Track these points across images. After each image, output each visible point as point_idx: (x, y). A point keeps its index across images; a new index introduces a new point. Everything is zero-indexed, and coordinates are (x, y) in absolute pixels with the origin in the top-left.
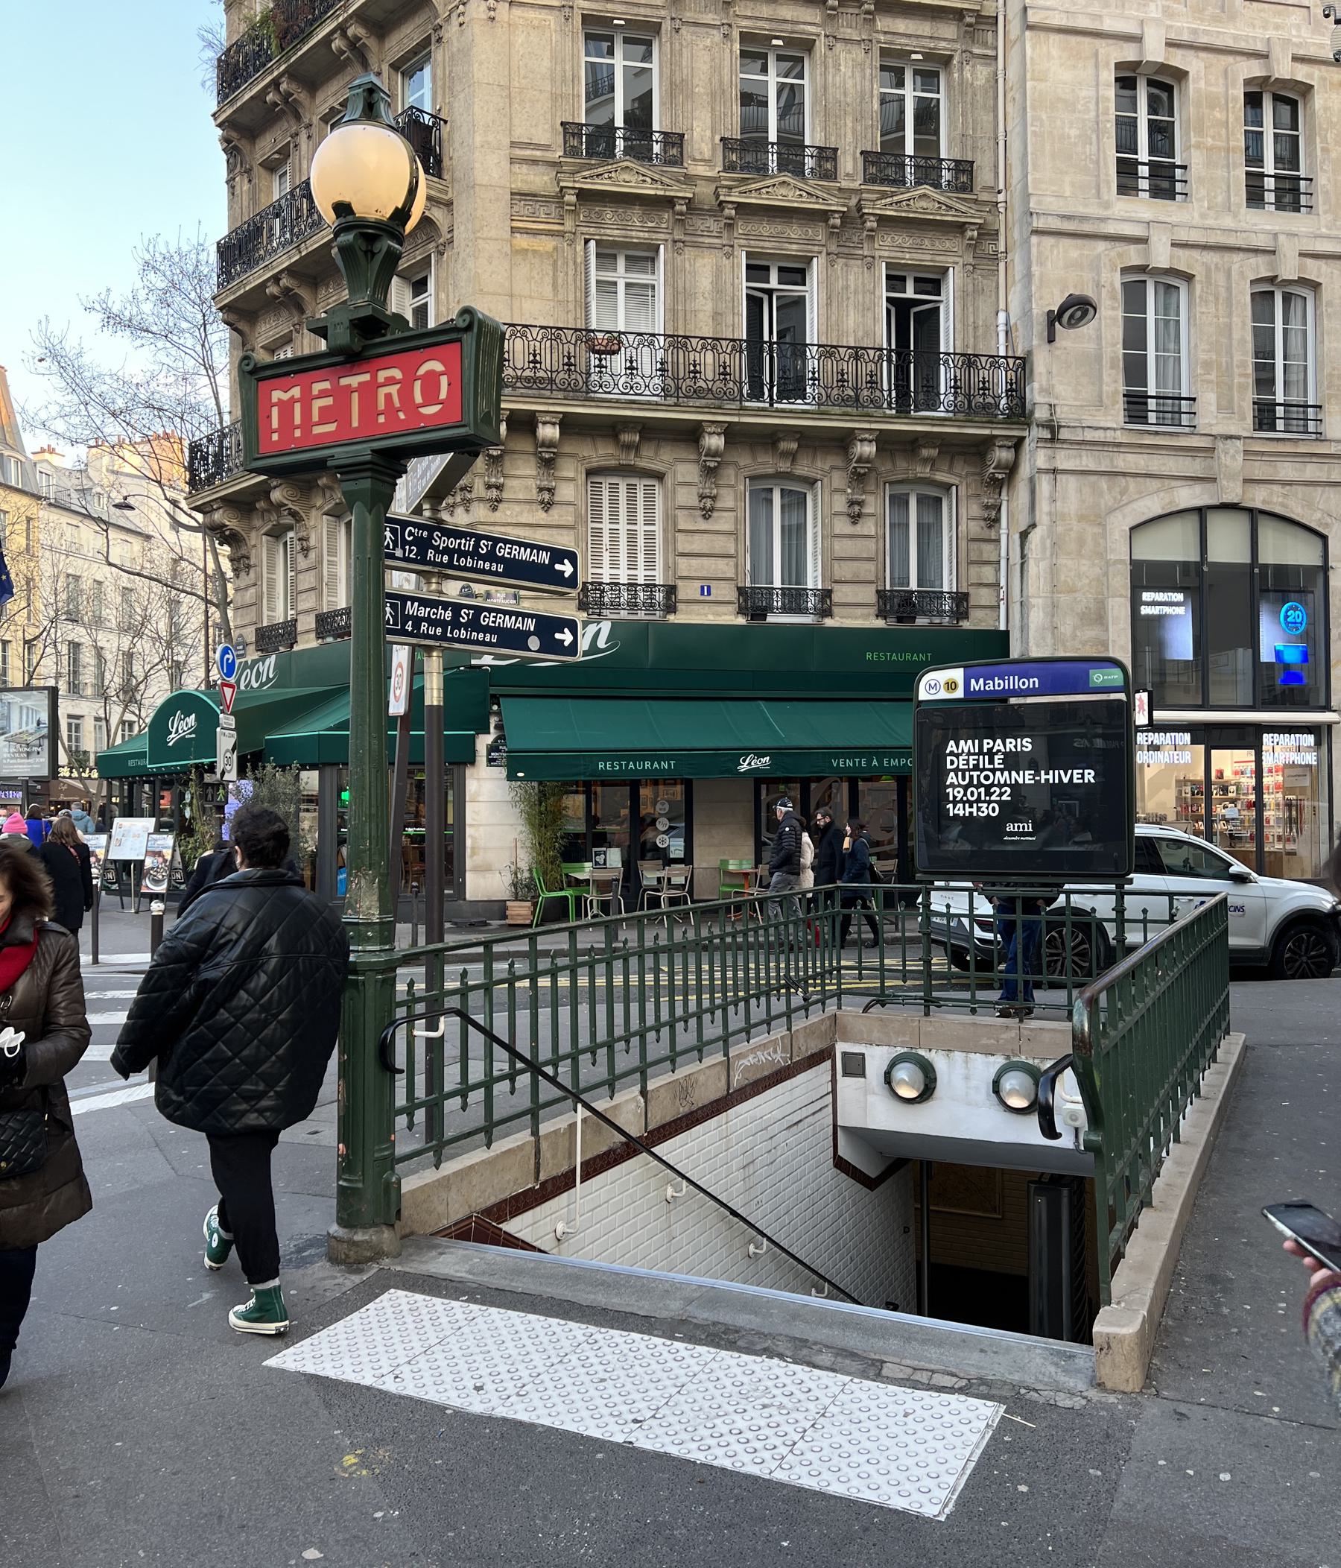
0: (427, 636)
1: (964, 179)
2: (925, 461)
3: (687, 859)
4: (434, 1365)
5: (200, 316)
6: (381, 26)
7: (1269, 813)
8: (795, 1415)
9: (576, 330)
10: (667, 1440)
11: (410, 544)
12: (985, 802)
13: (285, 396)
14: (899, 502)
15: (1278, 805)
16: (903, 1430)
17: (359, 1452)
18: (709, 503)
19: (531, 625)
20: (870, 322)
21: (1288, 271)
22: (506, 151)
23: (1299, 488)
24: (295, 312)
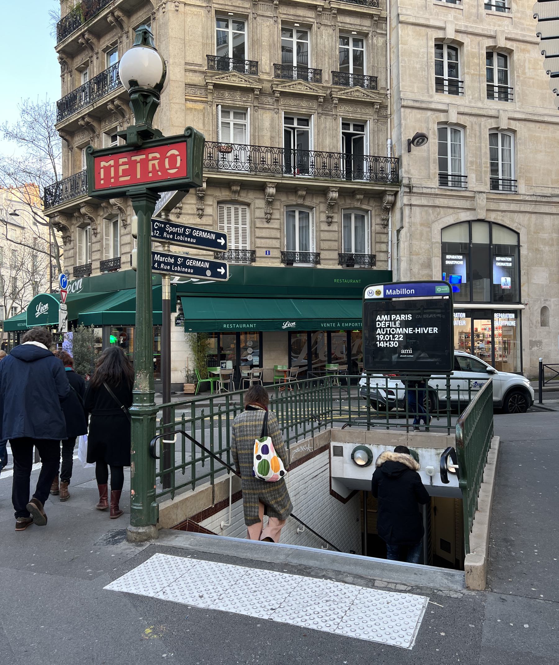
0: (164, 270)
1: (373, 84)
2: (358, 200)
3: (260, 365)
4: (190, 588)
5: (47, 134)
6: (129, 12)
7: (496, 346)
8: (340, 605)
9: (213, 142)
10: (287, 617)
11: (157, 230)
12: (392, 341)
13: (107, 164)
14: (347, 217)
15: (500, 342)
16: (387, 607)
17: (152, 627)
18: (269, 216)
19: (207, 265)
20: (335, 142)
21: (504, 126)
22: (183, 67)
23: (508, 213)
24: (91, 133)
